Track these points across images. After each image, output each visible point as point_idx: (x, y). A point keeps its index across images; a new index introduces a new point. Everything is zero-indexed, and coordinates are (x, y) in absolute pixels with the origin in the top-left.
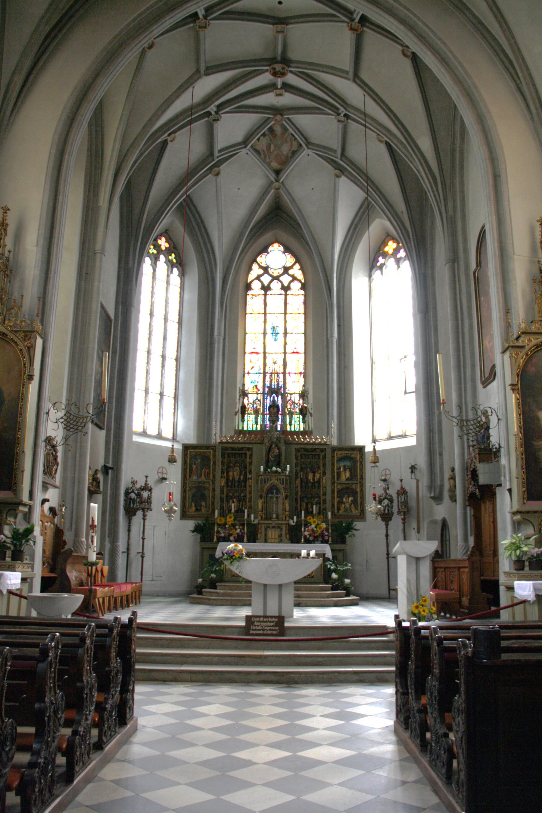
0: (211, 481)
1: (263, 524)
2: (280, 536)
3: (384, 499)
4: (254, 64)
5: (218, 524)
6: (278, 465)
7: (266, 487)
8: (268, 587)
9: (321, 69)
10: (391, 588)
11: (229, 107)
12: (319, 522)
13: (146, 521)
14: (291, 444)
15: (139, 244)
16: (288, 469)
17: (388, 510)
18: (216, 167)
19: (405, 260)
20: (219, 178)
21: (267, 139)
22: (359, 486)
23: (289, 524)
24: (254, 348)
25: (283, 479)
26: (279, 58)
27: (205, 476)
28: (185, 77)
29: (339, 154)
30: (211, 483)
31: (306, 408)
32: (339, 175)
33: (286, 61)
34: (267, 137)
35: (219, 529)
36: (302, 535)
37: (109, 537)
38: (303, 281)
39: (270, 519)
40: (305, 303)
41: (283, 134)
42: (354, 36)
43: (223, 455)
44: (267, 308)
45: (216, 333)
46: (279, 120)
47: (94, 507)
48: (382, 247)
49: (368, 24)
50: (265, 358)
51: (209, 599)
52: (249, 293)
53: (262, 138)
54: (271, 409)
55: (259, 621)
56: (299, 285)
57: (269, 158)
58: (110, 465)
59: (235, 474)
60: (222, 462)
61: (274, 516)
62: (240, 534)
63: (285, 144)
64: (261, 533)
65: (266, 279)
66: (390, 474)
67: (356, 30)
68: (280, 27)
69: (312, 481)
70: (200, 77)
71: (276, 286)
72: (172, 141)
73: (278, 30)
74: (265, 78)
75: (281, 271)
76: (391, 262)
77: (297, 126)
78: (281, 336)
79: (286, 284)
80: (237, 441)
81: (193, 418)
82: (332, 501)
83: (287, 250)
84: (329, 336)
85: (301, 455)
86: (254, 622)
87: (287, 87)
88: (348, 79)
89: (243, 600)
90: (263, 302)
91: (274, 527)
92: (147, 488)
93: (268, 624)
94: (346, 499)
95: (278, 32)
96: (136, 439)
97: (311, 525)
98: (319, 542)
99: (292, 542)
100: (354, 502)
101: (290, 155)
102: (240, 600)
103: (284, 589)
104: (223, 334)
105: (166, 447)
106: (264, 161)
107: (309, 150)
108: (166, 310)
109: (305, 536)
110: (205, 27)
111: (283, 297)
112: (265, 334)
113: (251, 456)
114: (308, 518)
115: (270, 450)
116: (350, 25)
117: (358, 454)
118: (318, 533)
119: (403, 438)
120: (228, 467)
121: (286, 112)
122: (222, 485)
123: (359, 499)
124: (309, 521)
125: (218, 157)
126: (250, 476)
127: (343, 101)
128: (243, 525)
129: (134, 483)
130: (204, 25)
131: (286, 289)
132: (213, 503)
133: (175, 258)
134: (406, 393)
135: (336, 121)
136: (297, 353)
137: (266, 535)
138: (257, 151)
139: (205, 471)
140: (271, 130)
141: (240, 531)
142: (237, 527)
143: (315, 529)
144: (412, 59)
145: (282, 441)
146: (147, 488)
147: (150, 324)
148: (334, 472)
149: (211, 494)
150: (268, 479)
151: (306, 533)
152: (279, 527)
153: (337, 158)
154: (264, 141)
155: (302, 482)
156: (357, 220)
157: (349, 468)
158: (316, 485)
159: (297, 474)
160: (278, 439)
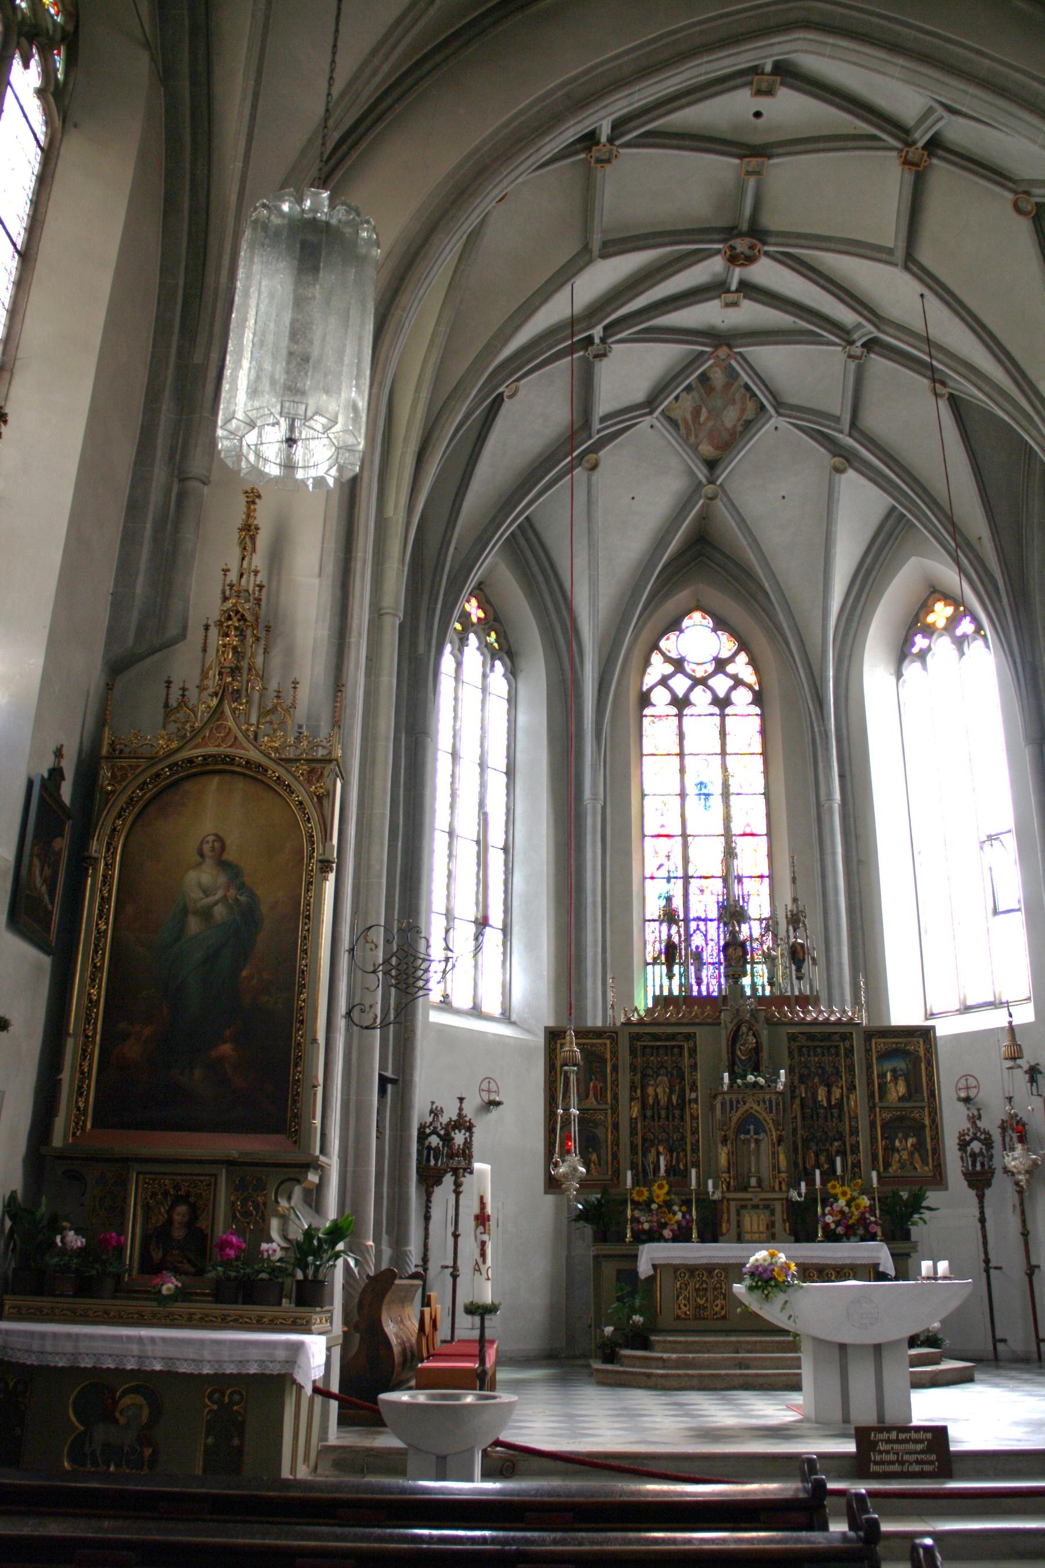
0: (608, 1107)
1: (734, 1199)
2: (771, 1225)
3: (971, 1140)
4: (691, 237)
5: (633, 1202)
6: (756, 1069)
7: (735, 1119)
8: (850, 1352)
9: (832, 246)
10: (999, 1336)
11: (628, 329)
12: (855, 1194)
13: (461, 1196)
14: (779, 1023)
15: (439, 606)
16: (783, 1079)
17: (982, 1165)
18: (591, 452)
19: (974, 639)
20: (596, 476)
21: (693, 398)
22: (927, 1114)
23: (789, 1201)
24: (663, 826)
25: (770, 1101)
26: (745, 227)
27: (596, 1098)
28: (560, 260)
29: (846, 425)
30: (609, 1111)
31: (802, 945)
32: (842, 467)
33: (757, 233)
34: (695, 393)
35: (637, 1213)
36: (817, 1221)
37: (387, 1233)
38: (757, 688)
39: (745, 1188)
40: (763, 732)
41: (728, 386)
42: (909, 178)
43: (633, 1051)
44: (686, 743)
45: (587, 793)
46: (723, 357)
47: (482, 1173)
48: (921, 615)
49: (940, 153)
50: (685, 846)
51: (649, 1376)
52: (647, 711)
53: (684, 394)
54: (730, 950)
55: (888, 1441)
56: (749, 696)
57: (696, 436)
58: (389, 1074)
59: (659, 1090)
60: (631, 1064)
61: (753, 1181)
62: (684, 1223)
63: (731, 408)
64: (728, 1221)
65: (680, 684)
66: (978, 1087)
67: (917, 165)
68: (754, 161)
69: (825, 1104)
70: (590, 262)
71: (701, 698)
72: (510, 397)
73: (750, 169)
74: (715, 266)
75: (710, 668)
76: (943, 645)
77: (759, 372)
78: (717, 801)
79: (721, 694)
80: (661, 1020)
81: (545, 973)
82: (872, 1146)
83: (721, 624)
84: (823, 798)
85: (800, 1048)
86: (876, 1443)
87: (749, 290)
88: (894, 264)
89: (727, 1375)
90: (676, 731)
91: (756, 1207)
92: (462, 1124)
93: (911, 1446)
94: (901, 1142)
95: (748, 173)
96: (436, 1017)
97: (836, 1200)
98: (858, 1238)
99: (797, 1241)
100: (920, 1146)
101: (739, 429)
102: (719, 1375)
103: (885, 1354)
104: (602, 796)
105: (495, 1034)
106: (686, 440)
107: (781, 418)
108: (482, 746)
109: (826, 1226)
110: (609, 161)
111: (717, 720)
112: (683, 795)
113: (693, 1052)
114: (829, 1185)
115: (735, 1038)
116: (904, 154)
117: (921, 1042)
118: (855, 1218)
119: (996, 1008)
120: (644, 1076)
121: (739, 342)
122: (634, 1116)
123: (928, 1140)
124: (832, 1191)
125: (599, 431)
126: (693, 1095)
127: (872, 311)
128: (687, 1203)
129: (435, 1112)
130: (605, 157)
131: (722, 703)
132: (615, 1156)
133: (497, 641)
134: (995, 912)
135: (844, 356)
136: (752, 835)
137: (739, 1224)
138: (673, 422)
139: (595, 1087)
140: (704, 378)
141: (684, 1216)
142: (676, 1208)
143: (846, 1209)
144: (1033, 218)
145: (762, 1019)
146: (462, 1124)
147: (453, 776)
148: (873, 1086)
149: (609, 1136)
150: (738, 1102)
151: (829, 1219)
152: (766, 1207)
153: (841, 432)
154: (688, 402)
155: (803, 1106)
156: (868, 561)
157: (904, 1075)
158: (835, 1111)
159: (793, 1091)
160: (754, 1013)
